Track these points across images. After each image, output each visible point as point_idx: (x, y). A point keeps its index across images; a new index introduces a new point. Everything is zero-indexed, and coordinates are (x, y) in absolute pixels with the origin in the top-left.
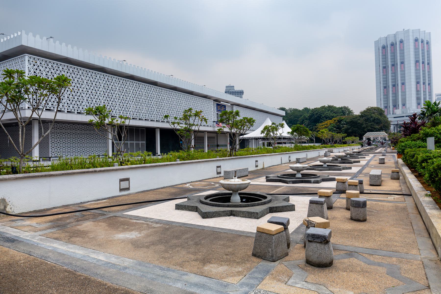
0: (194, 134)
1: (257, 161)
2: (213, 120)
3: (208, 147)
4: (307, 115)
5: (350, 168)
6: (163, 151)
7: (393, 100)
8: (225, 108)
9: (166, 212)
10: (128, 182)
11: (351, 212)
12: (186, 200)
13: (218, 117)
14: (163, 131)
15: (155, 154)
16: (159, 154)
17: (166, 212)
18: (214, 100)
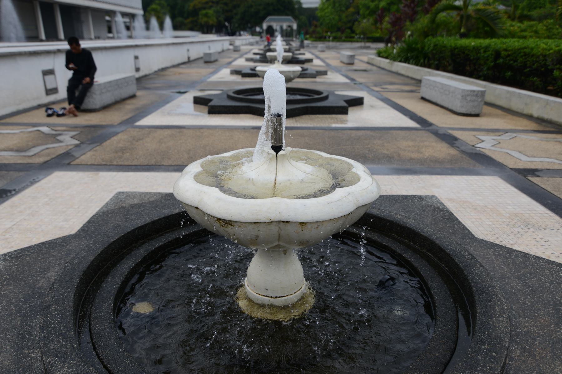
10: (49, 87)
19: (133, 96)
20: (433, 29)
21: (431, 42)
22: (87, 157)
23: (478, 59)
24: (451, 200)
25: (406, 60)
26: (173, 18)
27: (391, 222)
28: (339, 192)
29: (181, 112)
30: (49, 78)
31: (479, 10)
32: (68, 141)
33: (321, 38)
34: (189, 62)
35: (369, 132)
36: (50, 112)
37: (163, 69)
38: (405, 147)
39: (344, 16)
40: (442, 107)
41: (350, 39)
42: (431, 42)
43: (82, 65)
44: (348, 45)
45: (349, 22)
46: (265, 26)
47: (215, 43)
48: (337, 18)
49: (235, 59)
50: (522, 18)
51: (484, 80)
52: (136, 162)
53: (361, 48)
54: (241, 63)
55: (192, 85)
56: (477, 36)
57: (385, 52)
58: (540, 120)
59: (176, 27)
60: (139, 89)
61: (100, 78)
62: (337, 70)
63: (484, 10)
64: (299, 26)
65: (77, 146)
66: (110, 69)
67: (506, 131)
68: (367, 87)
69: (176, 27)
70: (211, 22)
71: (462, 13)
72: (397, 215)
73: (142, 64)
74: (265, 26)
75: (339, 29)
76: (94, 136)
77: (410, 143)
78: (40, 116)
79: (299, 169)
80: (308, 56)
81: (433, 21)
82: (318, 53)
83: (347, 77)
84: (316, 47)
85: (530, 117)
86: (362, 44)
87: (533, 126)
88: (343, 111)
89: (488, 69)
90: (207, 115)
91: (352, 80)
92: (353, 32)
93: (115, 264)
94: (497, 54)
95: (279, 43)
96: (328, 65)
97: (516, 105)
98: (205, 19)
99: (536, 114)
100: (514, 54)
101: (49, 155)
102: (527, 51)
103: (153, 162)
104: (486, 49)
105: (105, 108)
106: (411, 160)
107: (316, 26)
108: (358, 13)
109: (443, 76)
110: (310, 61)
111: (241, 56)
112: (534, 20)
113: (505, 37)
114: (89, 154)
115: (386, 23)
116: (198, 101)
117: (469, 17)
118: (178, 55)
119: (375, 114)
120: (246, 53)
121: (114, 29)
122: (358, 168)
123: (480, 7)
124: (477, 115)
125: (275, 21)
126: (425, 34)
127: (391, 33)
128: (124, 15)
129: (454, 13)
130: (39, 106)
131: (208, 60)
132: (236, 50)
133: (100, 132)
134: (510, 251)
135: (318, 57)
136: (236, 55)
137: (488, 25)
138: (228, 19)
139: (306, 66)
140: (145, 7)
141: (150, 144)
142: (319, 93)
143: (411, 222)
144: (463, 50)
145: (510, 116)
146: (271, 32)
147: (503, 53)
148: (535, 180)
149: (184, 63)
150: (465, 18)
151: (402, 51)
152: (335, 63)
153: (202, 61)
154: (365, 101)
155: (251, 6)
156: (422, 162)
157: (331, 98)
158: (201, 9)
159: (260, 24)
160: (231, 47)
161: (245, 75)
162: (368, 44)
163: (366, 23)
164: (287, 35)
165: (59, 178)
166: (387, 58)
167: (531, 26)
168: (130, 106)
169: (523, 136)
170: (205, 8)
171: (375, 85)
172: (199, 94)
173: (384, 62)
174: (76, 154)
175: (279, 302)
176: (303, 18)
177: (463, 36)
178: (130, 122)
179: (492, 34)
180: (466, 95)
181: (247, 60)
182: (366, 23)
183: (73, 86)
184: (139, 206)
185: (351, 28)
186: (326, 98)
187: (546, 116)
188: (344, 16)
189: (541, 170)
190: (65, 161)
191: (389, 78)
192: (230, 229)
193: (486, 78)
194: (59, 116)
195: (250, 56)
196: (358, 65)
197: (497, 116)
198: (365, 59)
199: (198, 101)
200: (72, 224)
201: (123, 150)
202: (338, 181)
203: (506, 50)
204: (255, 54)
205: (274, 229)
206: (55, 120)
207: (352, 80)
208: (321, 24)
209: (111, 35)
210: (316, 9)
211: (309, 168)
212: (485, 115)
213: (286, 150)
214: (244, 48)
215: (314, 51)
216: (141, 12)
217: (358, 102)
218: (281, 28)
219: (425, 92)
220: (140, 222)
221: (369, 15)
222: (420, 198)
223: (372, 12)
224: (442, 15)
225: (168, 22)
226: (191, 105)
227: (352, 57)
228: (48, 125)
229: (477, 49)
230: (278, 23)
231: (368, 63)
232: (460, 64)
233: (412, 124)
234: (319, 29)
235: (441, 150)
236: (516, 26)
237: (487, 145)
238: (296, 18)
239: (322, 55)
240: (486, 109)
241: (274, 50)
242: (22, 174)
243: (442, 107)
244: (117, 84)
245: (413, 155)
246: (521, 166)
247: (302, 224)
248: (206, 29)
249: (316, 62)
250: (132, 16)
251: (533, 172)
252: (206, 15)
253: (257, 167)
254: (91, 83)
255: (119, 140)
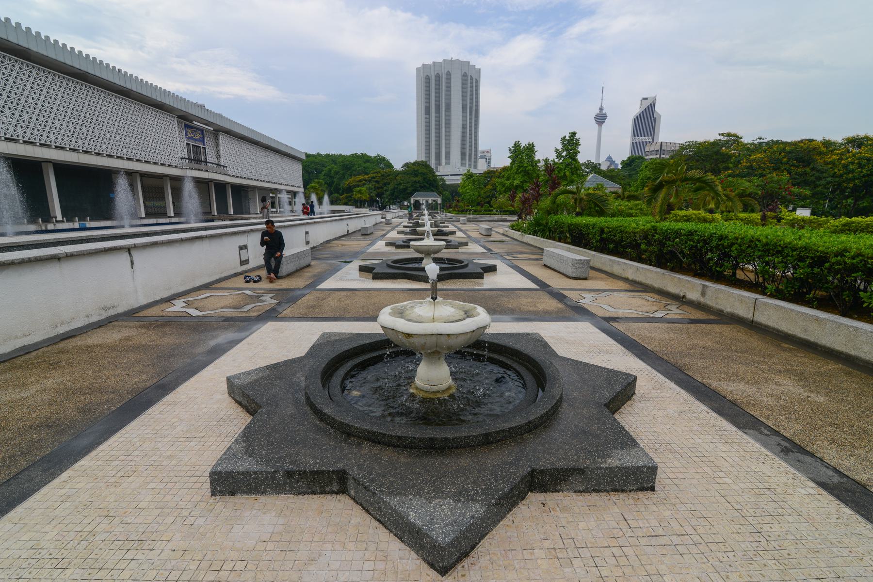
0: (142, 181)
1: (307, 233)
2: (180, 155)
3: (174, 206)
4: (341, 160)
5: (423, 239)
6: (68, 215)
7: (436, 105)
8: (203, 134)
9: (247, 292)
10: (243, 259)
11: (252, 422)
12: (443, 243)
13: (189, 151)
14: (63, 170)
15: (48, 217)
16: (60, 218)
17: (247, 292)
18: (179, 117)
19: (309, 266)
20: (555, 209)
21: (552, 219)
22: (287, 312)
23: (589, 234)
24: (552, 337)
25: (535, 233)
26: (330, 195)
27: (505, 347)
28: (468, 320)
29: (349, 278)
30: (243, 252)
31: (589, 194)
32: (269, 301)
33: (463, 212)
34: (348, 235)
35: (499, 292)
36: (248, 279)
37: (328, 242)
38: (526, 302)
39: (482, 192)
40: (559, 272)
41: (489, 212)
42: (552, 219)
43: (273, 242)
44: (487, 217)
45: (488, 197)
46: (412, 201)
47: (370, 218)
48: (477, 194)
49: (389, 232)
50: (630, 198)
51: (595, 251)
52: (324, 315)
53: (498, 220)
54: (393, 235)
55: (355, 255)
56: (590, 215)
57: (517, 225)
58: (633, 282)
59: (332, 203)
60: (314, 258)
61: (287, 252)
62: (476, 241)
63: (594, 194)
64: (443, 200)
65: (277, 304)
66: (294, 244)
67: (604, 291)
68: (501, 257)
69: (332, 203)
70: (364, 198)
71: (576, 196)
72: (510, 343)
73: (311, 238)
74: (412, 201)
75: (478, 204)
76: (287, 297)
77: (530, 300)
78: (240, 282)
79: (446, 309)
80: (452, 228)
81: (554, 202)
82: (460, 226)
83: (484, 247)
84: (459, 220)
85: (626, 280)
86: (500, 217)
87: (626, 286)
88: (480, 276)
89: (597, 242)
90: (371, 280)
91: (489, 250)
92: (491, 206)
93: (337, 369)
94: (602, 231)
95: (426, 218)
96: (469, 237)
97: (617, 270)
98: (359, 195)
99: (631, 277)
100: (613, 231)
101: (259, 310)
102: (622, 229)
103: (338, 315)
104: (594, 226)
105: (289, 275)
106: (528, 312)
107: (458, 201)
108: (495, 189)
109: (562, 248)
110: (454, 233)
111: (393, 229)
112: (640, 200)
113: (613, 215)
114: (289, 310)
115: (517, 202)
116: (362, 269)
117: (581, 200)
118: (339, 228)
119: (506, 278)
120: (397, 226)
121: (277, 205)
122: (480, 310)
123: (591, 191)
124: (585, 279)
125: (421, 196)
126: (549, 213)
127: (522, 210)
128: (288, 192)
129: (571, 196)
130: (236, 275)
131: (365, 233)
132: (388, 223)
133: (291, 294)
134: (577, 362)
135: (460, 230)
136: (388, 228)
137: (598, 206)
138: (379, 195)
139: (449, 238)
140: (305, 185)
141: (332, 302)
142: (460, 262)
143: (517, 346)
144: (577, 226)
145: (611, 279)
146: (417, 206)
147: (606, 230)
148: (614, 324)
149: (344, 236)
150: (578, 201)
151: (530, 224)
152: (474, 235)
153: (360, 233)
154: (498, 268)
155: (400, 184)
156: (536, 313)
157: (470, 265)
158: (355, 186)
159: (407, 198)
160: (383, 220)
161: (398, 247)
162: (504, 217)
163: (502, 199)
164: (433, 208)
165: (270, 327)
166: (519, 231)
167: (636, 205)
168: (308, 274)
169: (616, 294)
170: (358, 186)
171: (508, 255)
172: (363, 263)
173: (517, 234)
174: (280, 310)
175: (436, 388)
176: (447, 193)
177: (578, 214)
178: (312, 286)
179: (601, 213)
180: (576, 263)
181: (399, 232)
182: (502, 199)
183: (268, 256)
184: (340, 340)
185: (489, 203)
186: (467, 266)
187: (637, 279)
188: (482, 192)
189: (621, 318)
190: (271, 315)
191: (519, 248)
192: (412, 340)
193: (596, 249)
194: (255, 282)
195: (401, 229)
196: (495, 236)
197: (601, 279)
198: (501, 231)
199: (362, 269)
200: (300, 351)
201: (313, 307)
202: (468, 314)
203: (607, 227)
204: (405, 227)
205: (434, 339)
206: (251, 285)
207: (489, 250)
208: (463, 199)
209: (274, 210)
210: (458, 185)
211: (453, 310)
212: (592, 278)
213: (439, 299)
214: (395, 221)
215: (456, 223)
216: (302, 190)
217: (492, 269)
218: (427, 202)
219: (547, 260)
220: (346, 348)
221: (505, 192)
222: (528, 334)
223: (508, 189)
224: (561, 198)
225: (326, 198)
226: (356, 273)
227: (490, 230)
228: (250, 289)
229: (587, 226)
230: (424, 198)
231: (503, 235)
232: (577, 238)
233: (533, 285)
234: (461, 204)
235: (552, 304)
236: (624, 205)
237: (587, 301)
238: (440, 193)
239: (464, 228)
240: (593, 273)
241: (423, 225)
242: (246, 323)
243: (559, 272)
244: (298, 256)
245: (530, 309)
246: (607, 315)
247: (448, 335)
248: (359, 203)
249: (459, 234)
250: (294, 194)
251: (615, 319)
252: (360, 192)
253: (423, 309)
254: (281, 256)
255: (309, 299)
